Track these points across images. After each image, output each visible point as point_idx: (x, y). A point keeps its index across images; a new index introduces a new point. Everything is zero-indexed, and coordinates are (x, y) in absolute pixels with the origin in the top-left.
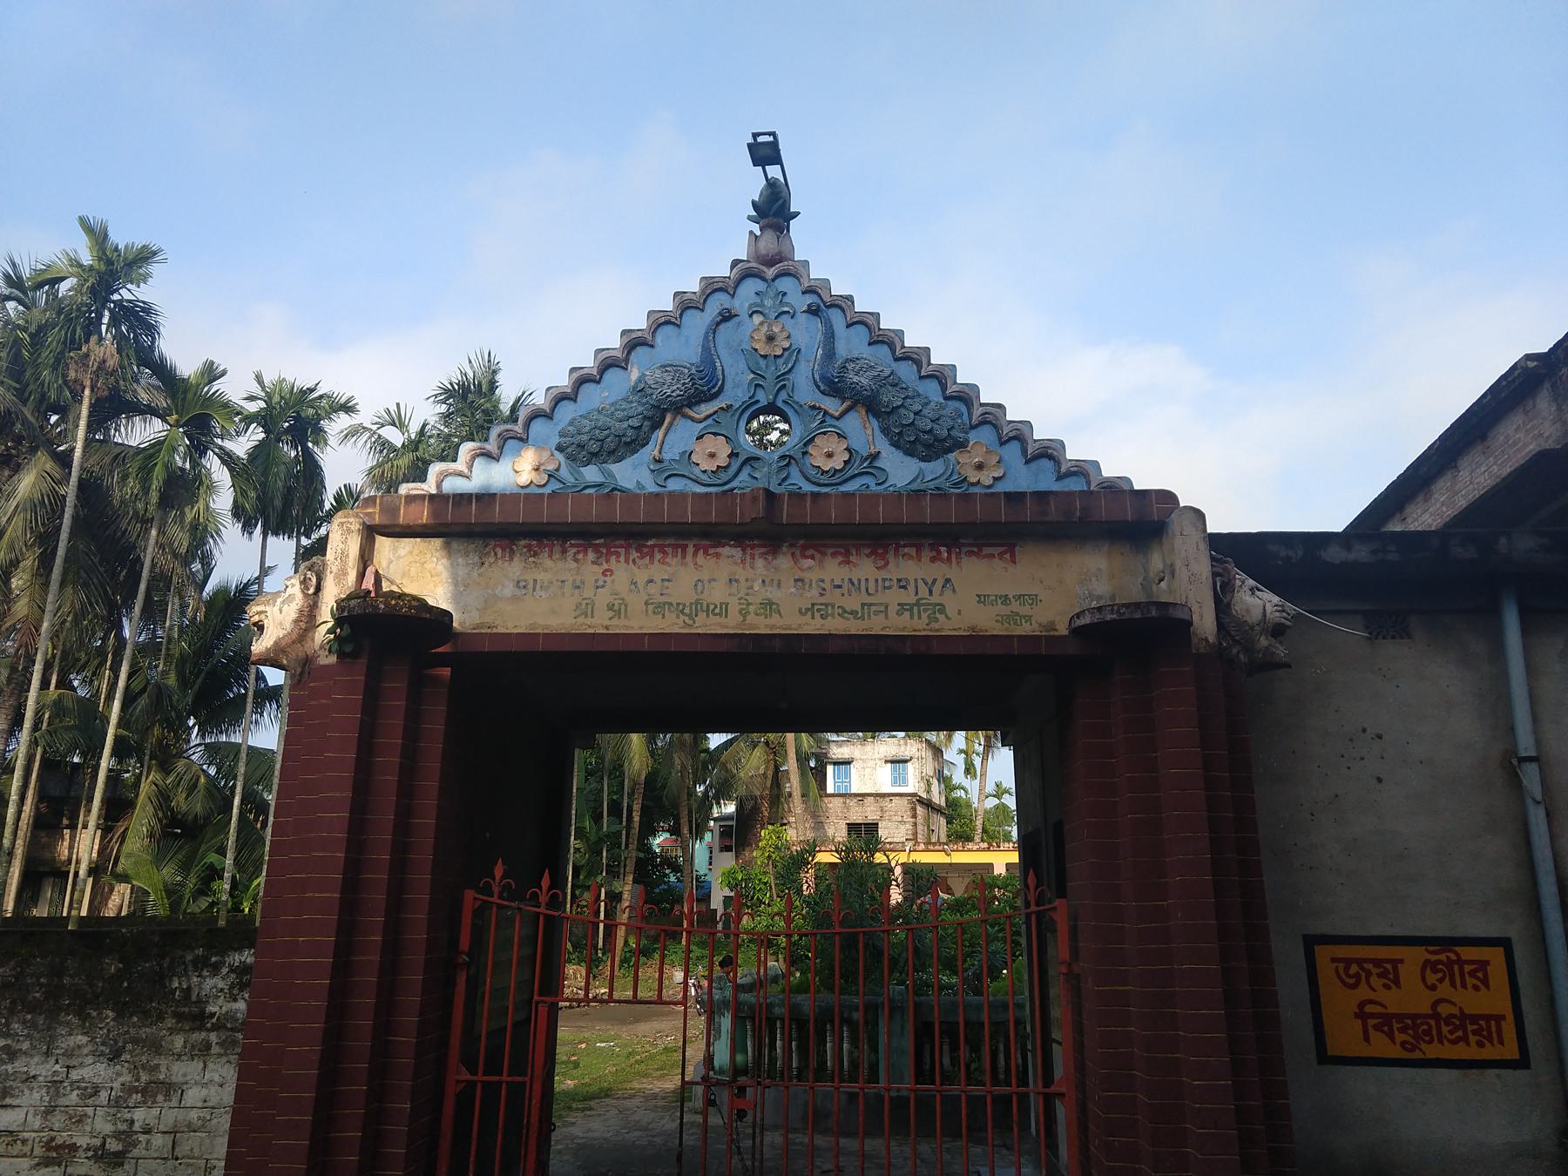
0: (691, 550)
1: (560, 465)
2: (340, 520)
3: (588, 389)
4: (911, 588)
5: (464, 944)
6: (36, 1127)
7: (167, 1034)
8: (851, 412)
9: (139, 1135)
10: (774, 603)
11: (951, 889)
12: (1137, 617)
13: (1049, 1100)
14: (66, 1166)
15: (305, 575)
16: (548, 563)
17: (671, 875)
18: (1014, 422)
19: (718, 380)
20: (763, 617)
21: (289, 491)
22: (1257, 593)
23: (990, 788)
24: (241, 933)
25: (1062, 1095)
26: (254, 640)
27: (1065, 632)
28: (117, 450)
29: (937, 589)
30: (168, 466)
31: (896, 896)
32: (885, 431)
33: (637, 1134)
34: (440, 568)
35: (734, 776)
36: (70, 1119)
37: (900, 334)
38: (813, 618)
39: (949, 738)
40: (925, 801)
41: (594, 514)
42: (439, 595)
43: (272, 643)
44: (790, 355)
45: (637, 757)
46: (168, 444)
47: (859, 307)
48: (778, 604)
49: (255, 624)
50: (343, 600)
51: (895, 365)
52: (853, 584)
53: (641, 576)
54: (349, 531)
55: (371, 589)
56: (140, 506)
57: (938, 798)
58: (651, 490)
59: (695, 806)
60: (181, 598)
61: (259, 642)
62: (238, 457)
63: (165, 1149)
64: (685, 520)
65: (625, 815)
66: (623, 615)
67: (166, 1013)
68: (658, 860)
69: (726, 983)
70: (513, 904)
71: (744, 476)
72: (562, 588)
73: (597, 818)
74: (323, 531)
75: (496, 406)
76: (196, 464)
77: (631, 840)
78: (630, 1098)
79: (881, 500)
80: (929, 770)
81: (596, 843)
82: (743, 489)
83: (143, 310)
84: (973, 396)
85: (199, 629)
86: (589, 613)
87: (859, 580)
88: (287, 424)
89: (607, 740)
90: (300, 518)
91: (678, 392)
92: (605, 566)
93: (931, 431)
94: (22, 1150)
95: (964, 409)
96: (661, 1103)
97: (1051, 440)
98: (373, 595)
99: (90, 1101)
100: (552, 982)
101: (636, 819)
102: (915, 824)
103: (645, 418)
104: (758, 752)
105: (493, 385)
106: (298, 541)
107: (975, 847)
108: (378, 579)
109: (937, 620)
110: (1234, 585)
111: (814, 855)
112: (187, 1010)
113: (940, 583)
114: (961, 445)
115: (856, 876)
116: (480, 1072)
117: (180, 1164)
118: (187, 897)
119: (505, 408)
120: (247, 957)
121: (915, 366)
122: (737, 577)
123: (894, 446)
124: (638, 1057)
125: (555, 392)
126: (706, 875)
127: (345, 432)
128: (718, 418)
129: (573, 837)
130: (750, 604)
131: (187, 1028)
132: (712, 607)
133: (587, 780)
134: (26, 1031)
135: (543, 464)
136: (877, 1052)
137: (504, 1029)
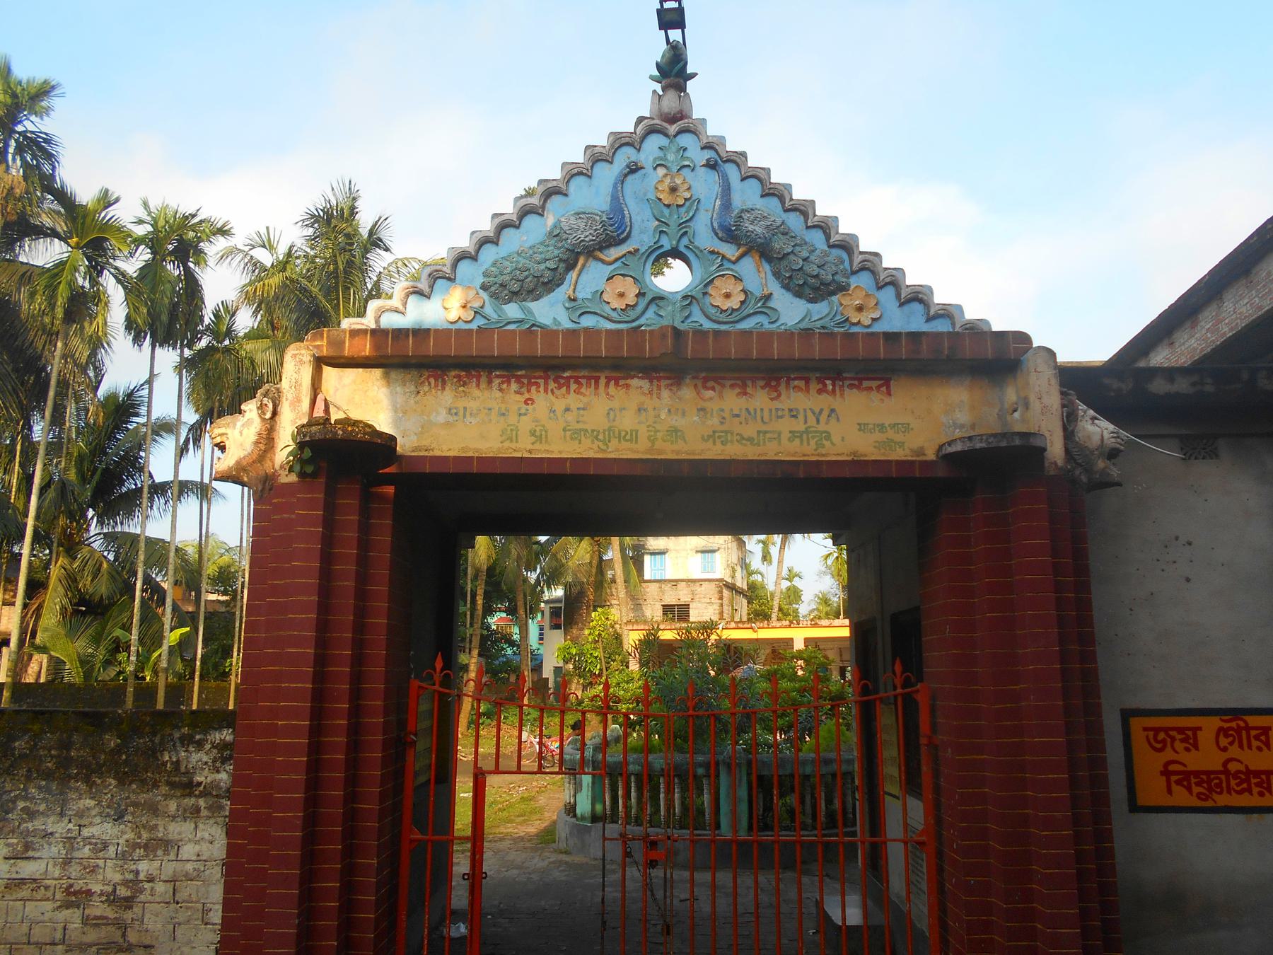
0: (603, 381)
1: (484, 303)
3: (508, 233)
4: (801, 417)
6: (56, 875)
10: (680, 431)
14: (84, 909)
16: (476, 392)
17: (508, 649)
18: (890, 269)
21: (175, 306)
22: (1096, 421)
23: (785, 573)
24: (225, 719)
28: (24, 269)
29: (823, 418)
30: (71, 283)
32: (777, 275)
33: (515, 872)
35: (563, 565)
36: (85, 869)
37: (788, 187)
38: (714, 443)
41: (517, 349)
42: (383, 422)
44: (691, 205)
45: (482, 548)
46: (70, 266)
47: (752, 162)
50: (303, 426)
51: (785, 216)
52: (750, 413)
53: (560, 405)
54: (301, 362)
56: (47, 320)
57: (741, 583)
63: (167, 895)
65: (469, 598)
66: (544, 440)
67: (160, 781)
71: (650, 313)
75: (356, 230)
76: (94, 283)
77: (475, 620)
80: (734, 558)
83: (46, 141)
84: (854, 245)
86: (514, 438)
87: (755, 410)
91: (591, 237)
92: (527, 396)
93: (817, 276)
94: (45, 895)
95: (845, 256)
96: (528, 845)
97: (921, 286)
99: (101, 855)
103: (561, 260)
105: (353, 211)
109: (823, 446)
110: (1077, 416)
112: (177, 779)
113: (826, 413)
114: (843, 289)
117: (181, 907)
120: (226, 735)
122: (645, 407)
124: (501, 806)
125: (479, 236)
127: (221, 254)
130: (659, 431)
131: (179, 794)
132: (623, 434)
134: (42, 795)
135: (469, 302)
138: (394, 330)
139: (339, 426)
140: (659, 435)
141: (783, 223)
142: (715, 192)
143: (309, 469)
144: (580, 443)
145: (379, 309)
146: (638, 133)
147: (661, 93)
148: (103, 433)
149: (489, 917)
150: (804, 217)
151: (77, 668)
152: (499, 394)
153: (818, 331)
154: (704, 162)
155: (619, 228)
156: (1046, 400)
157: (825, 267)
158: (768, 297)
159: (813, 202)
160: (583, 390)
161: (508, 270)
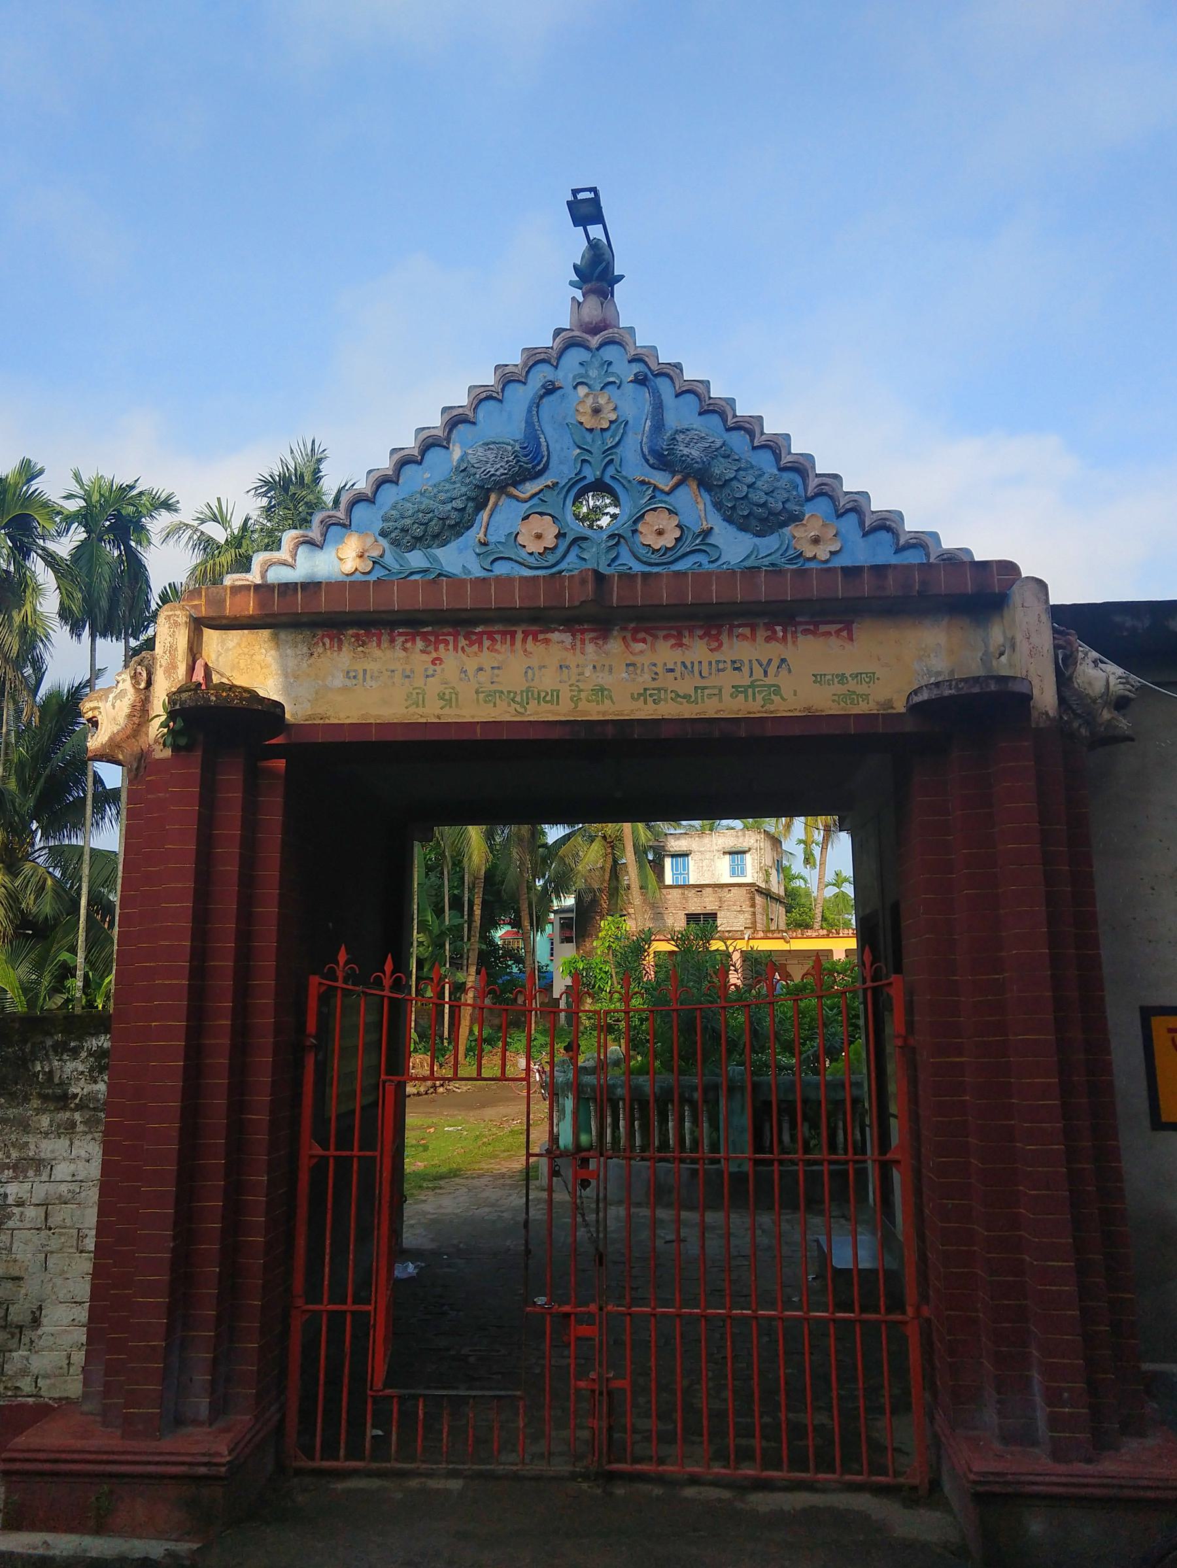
0: (519, 636)
1: (384, 551)
2: (166, 613)
3: (409, 470)
4: (746, 669)
5: (311, 1025)
7: (34, 1114)
8: (682, 487)
9: (13, 1207)
11: (790, 976)
12: (976, 692)
13: (885, 1169)
15: (135, 669)
16: (377, 653)
17: (514, 966)
18: (852, 493)
19: (543, 457)
20: (595, 703)
21: (115, 592)
22: (1100, 665)
24: (99, 1023)
25: (897, 1162)
26: (90, 736)
27: (903, 710)
29: (772, 670)
31: (734, 979)
32: (718, 506)
33: (487, 1210)
34: (269, 659)
38: (645, 703)
39: (788, 827)
40: (764, 891)
41: (420, 601)
42: (269, 687)
43: (107, 739)
44: (617, 429)
45: (476, 852)
48: (609, 690)
49: (89, 720)
50: (174, 693)
51: (726, 436)
52: (686, 667)
53: (471, 664)
54: (176, 624)
55: (202, 681)
57: (777, 888)
58: (478, 575)
59: (534, 900)
60: (16, 703)
61: (94, 738)
62: (61, 557)
63: (39, 1220)
64: (513, 606)
65: (466, 909)
67: (31, 1094)
68: (501, 952)
69: (569, 1066)
70: (358, 988)
71: (572, 557)
72: (392, 677)
73: (439, 912)
74: (150, 632)
76: (20, 567)
77: (473, 933)
78: (478, 1178)
79: (714, 578)
80: (768, 860)
81: (438, 936)
82: (571, 571)
84: (808, 466)
85: (35, 733)
86: (421, 702)
87: (692, 663)
88: (108, 523)
89: (446, 833)
90: (127, 620)
92: (434, 655)
93: (764, 505)
95: (799, 480)
96: (508, 1182)
98: (203, 687)
100: (397, 1063)
101: (478, 912)
102: (754, 914)
104: (596, 846)
105: (316, 477)
106: (127, 642)
107: (815, 934)
108: (207, 669)
110: (1076, 658)
111: (650, 944)
112: (50, 1091)
113: (775, 663)
114: (796, 518)
115: (693, 961)
116: (332, 1147)
117: (53, 1233)
118: (43, 994)
119: (329, 499)
120: (104, 1042)
121: (748, 436)
122: (567, 664)
123: (727, 521)
124: (485, 1140)
125: (376, 475)
126: (547, 966)
128: (544, 496)
129: (415, 931)
130: (582, 690)
132: (543, 694)
133: (427, 875)
135: (367, 551)
136: (717, 1129)
137: (353, 1111)
138: (280, 585)
139: (212, 692)
140: (583, 695)
141: (724, 444)
142: (646, 411)
143: (182, 741)
144: (495, 706)
145: (265, 562)
146: (555, 348)
147: (581, 299)
148: (46, 737)
149: (445, 1257)
150: (750, 436)
151: (19, 996)
152: (403, 654)
153: (764, 568)
154: (631, 378)
155: (534, 458)
156: (1035, 640)
157: (775, 494)
158: (708, 532)
159: (760, 419)
160: (498, 647)
161: (410, 512)
